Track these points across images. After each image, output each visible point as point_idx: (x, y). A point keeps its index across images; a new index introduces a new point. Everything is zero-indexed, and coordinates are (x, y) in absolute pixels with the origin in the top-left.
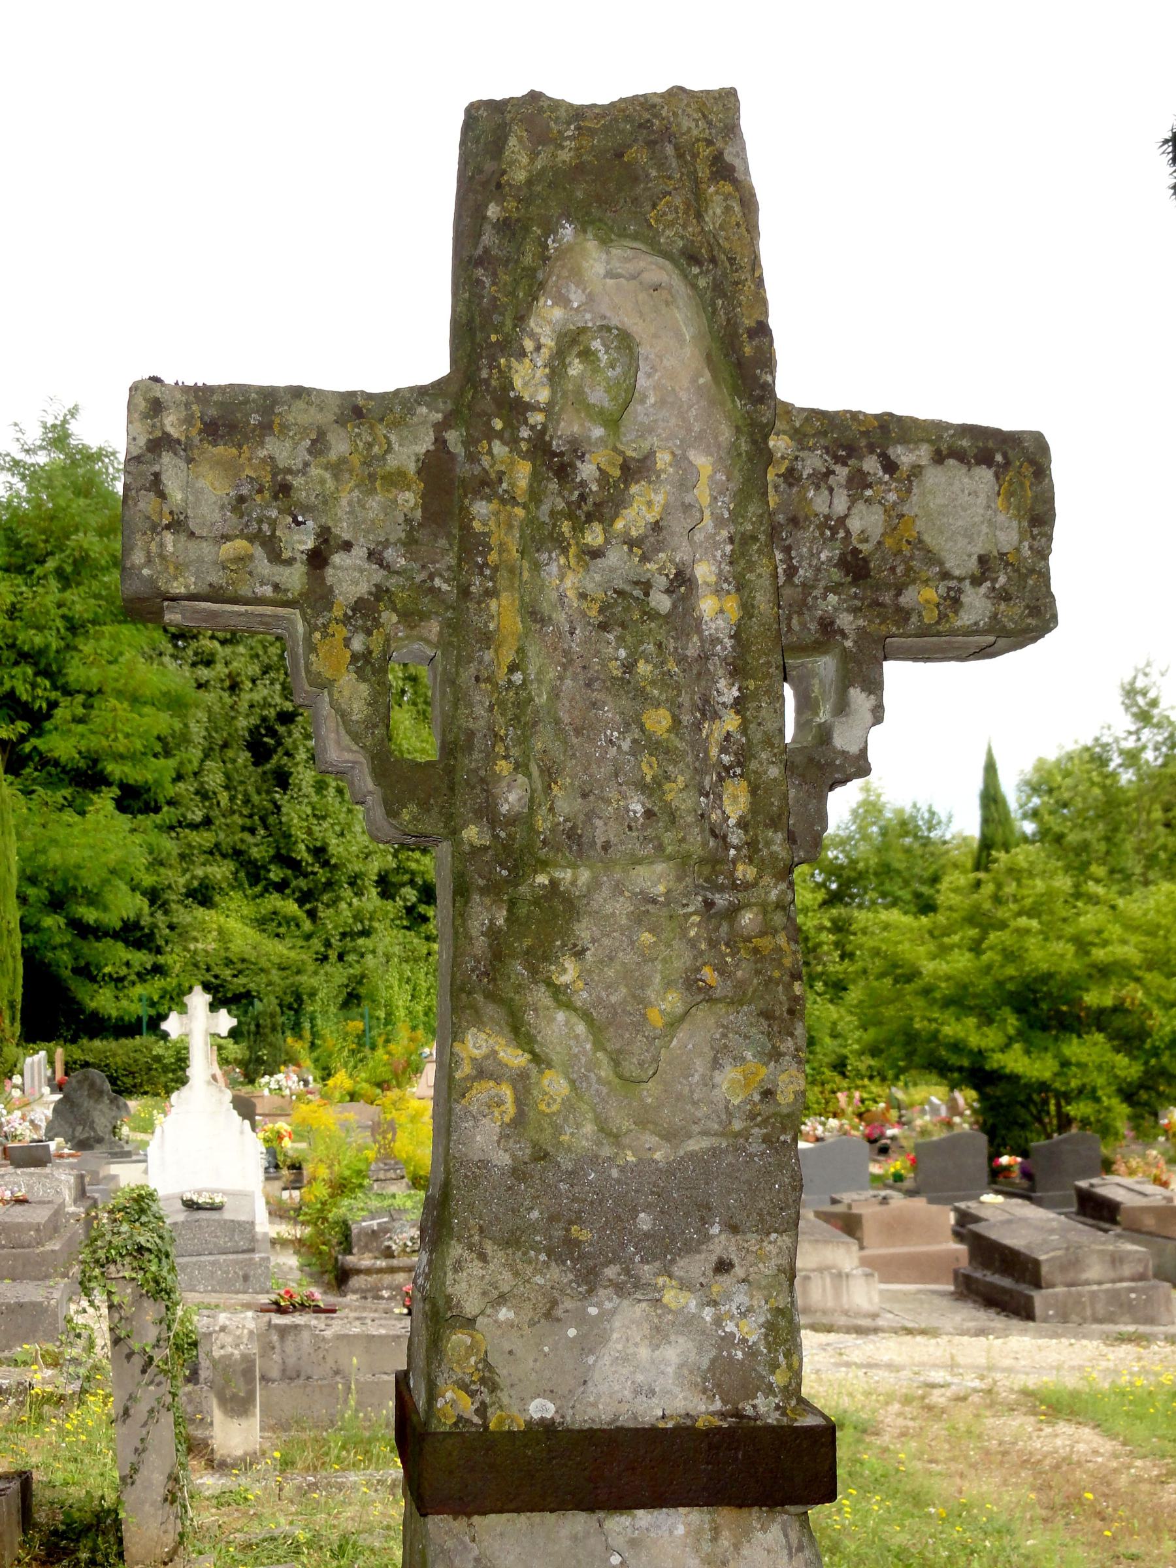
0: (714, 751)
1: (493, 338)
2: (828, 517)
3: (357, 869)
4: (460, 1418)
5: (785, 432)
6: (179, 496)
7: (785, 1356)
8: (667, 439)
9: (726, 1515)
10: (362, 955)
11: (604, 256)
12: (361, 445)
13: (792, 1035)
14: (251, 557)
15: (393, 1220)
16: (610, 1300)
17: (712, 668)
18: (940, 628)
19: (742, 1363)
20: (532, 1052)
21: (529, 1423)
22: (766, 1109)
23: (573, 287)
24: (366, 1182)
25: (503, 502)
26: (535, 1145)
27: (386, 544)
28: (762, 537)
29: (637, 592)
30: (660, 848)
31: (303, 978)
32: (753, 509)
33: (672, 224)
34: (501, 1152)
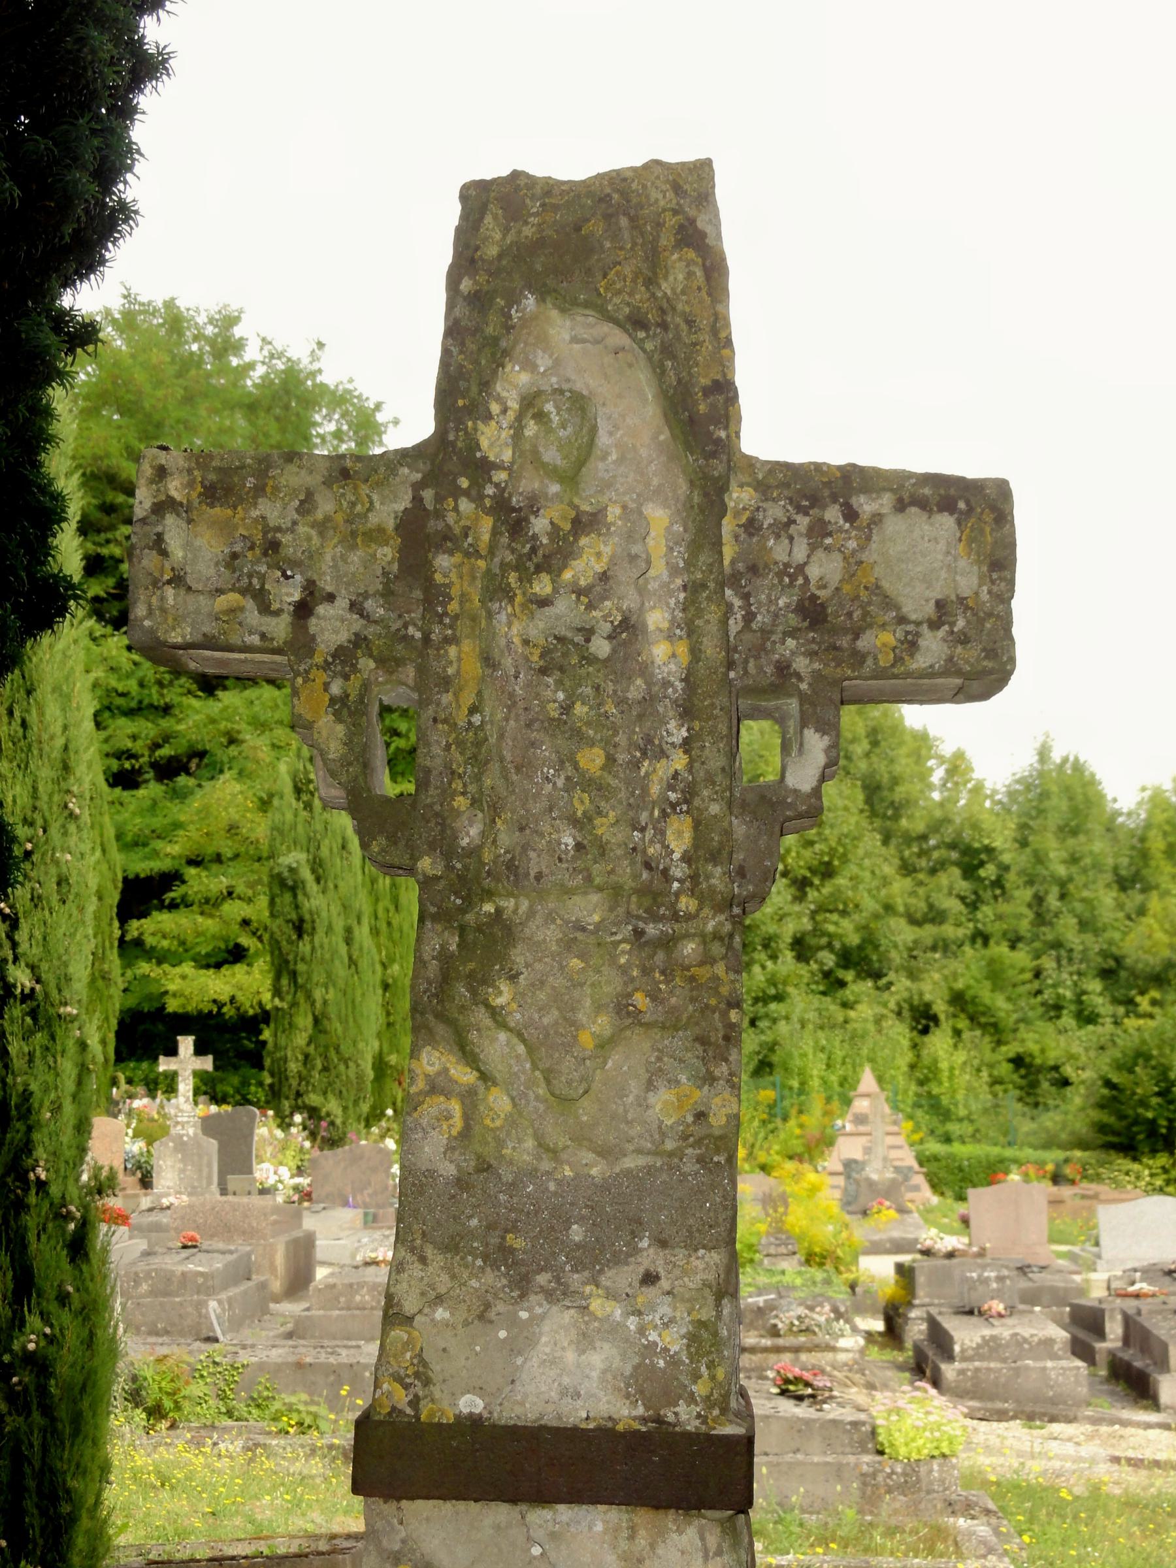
0: (655, 789)
1: (460, 403)
2: (787, 565)
3: (771, 931)
4: (394, 1408)
5: (749, 485)
6: (180, 554)
7: (708, 1367)
8: (624, 494)
9: (643, 1516)
10: (775, 1021)
11: (568, 323)
12: (345, 504)
13: (726, 1060)
14: (242, 609)
15: (781, 1297)
16: (541, 1305)
17: (661, 710)
18: (895, 671)
19: (663, 1371)
20: (479, 1070)
21: (458, 1417)
22: (698, 1131)
23: (540, 353)
24: (757, 1256)
25: (467, 555)
26: (479, 1157)
27: (366, 595)
28: (712, 585)
29: (579, 639)
30: (589, 879)
32: (704, 558)
33: (619, 292)
34: (447, 1163)
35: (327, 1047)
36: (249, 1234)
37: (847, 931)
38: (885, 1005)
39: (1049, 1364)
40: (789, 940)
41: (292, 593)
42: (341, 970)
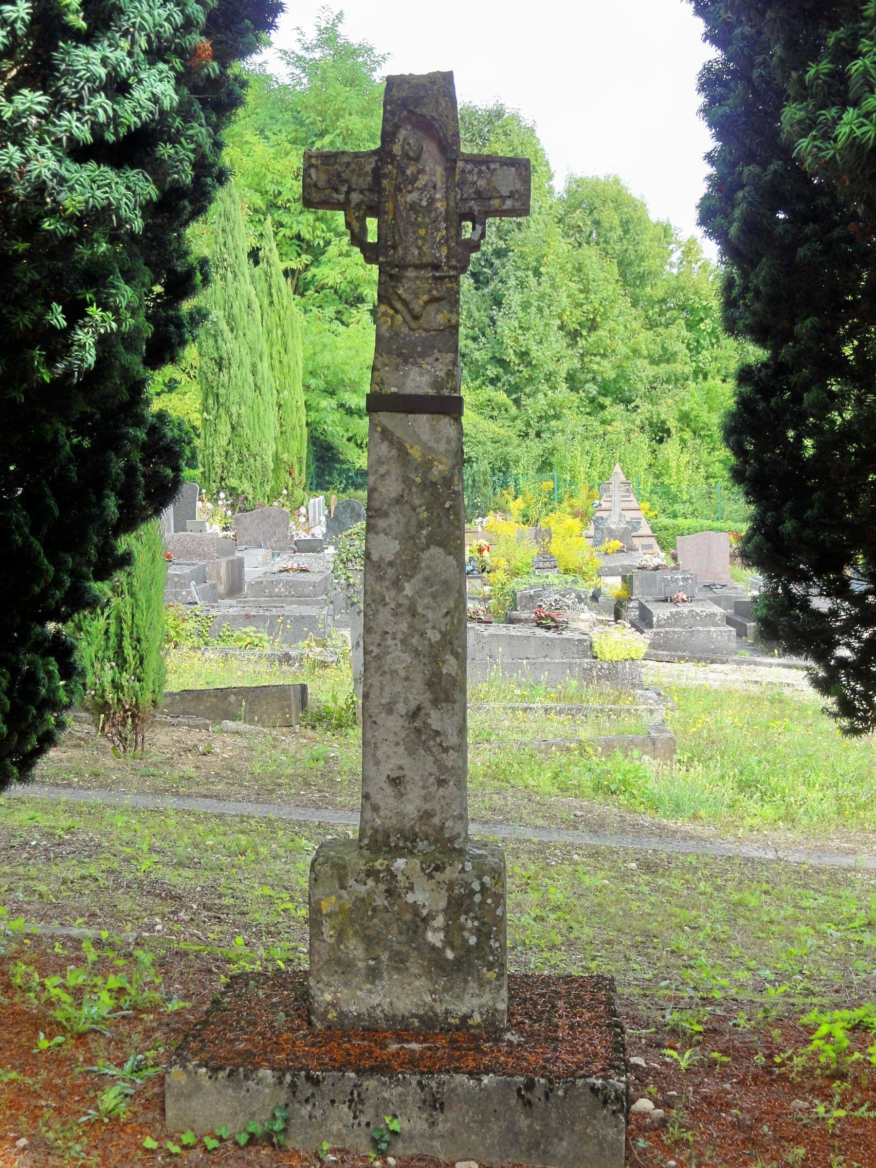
10: (554, 433)
31: (509, 449)
35: (240, 446)
36: (204, 556)
37: (606, 369)
38: (633, 422)
39: (712, 629)
40: (564, 376)
41: (345, 189)
42: (249, 393)
